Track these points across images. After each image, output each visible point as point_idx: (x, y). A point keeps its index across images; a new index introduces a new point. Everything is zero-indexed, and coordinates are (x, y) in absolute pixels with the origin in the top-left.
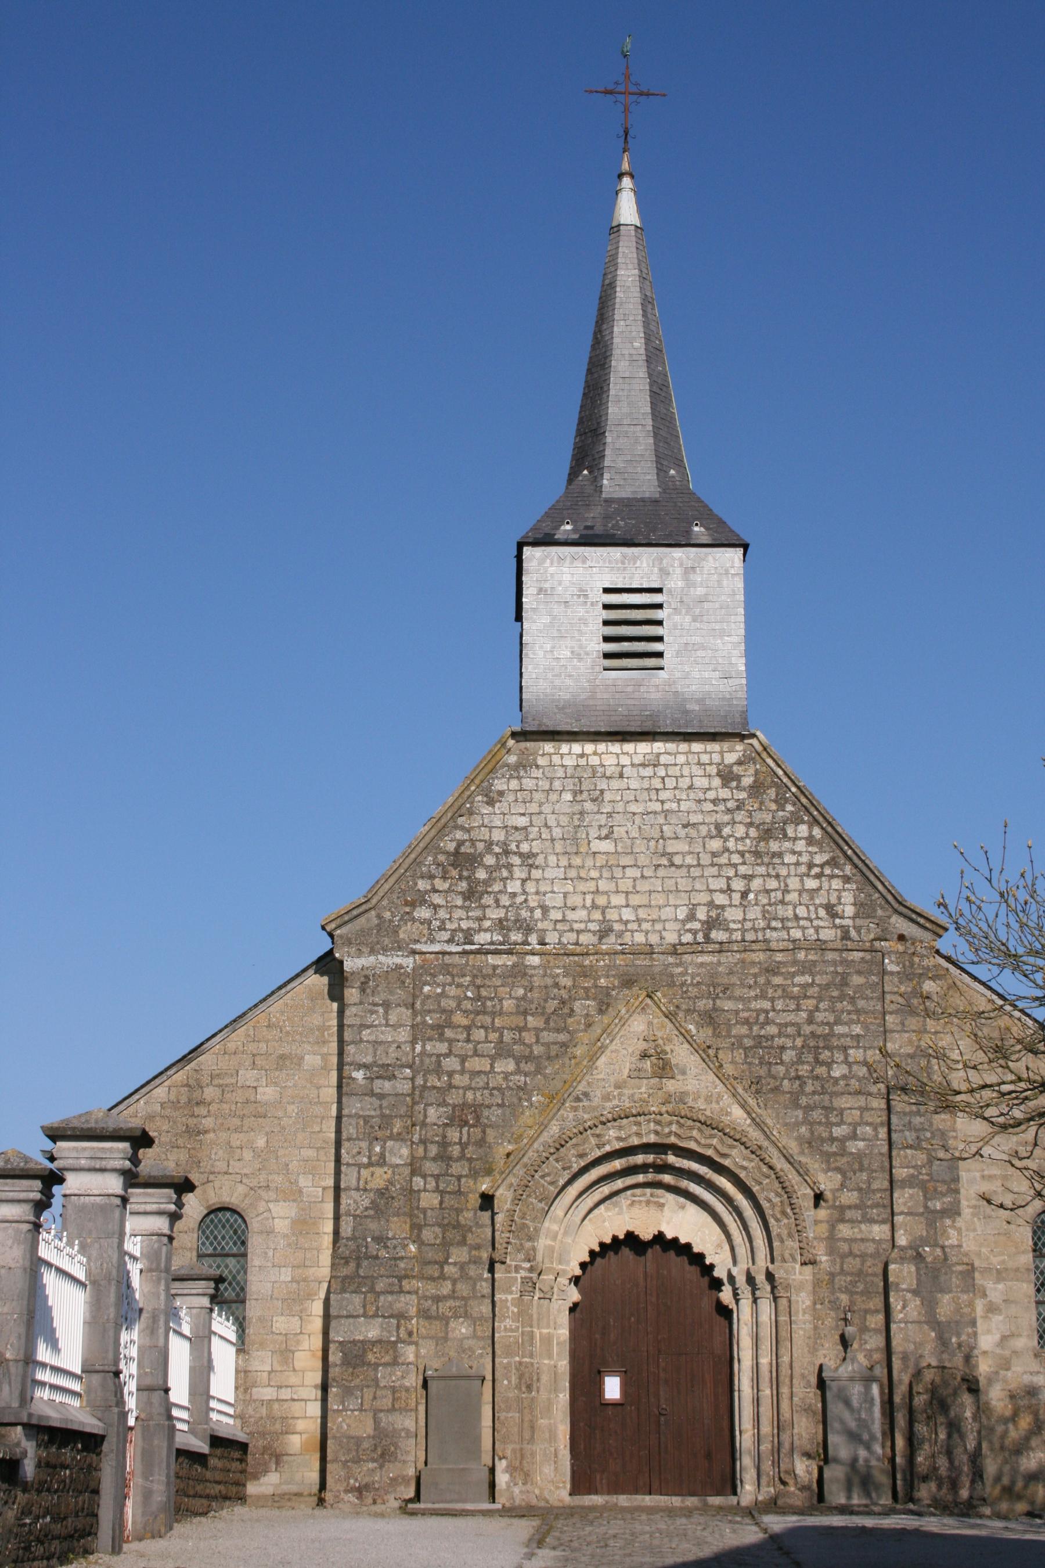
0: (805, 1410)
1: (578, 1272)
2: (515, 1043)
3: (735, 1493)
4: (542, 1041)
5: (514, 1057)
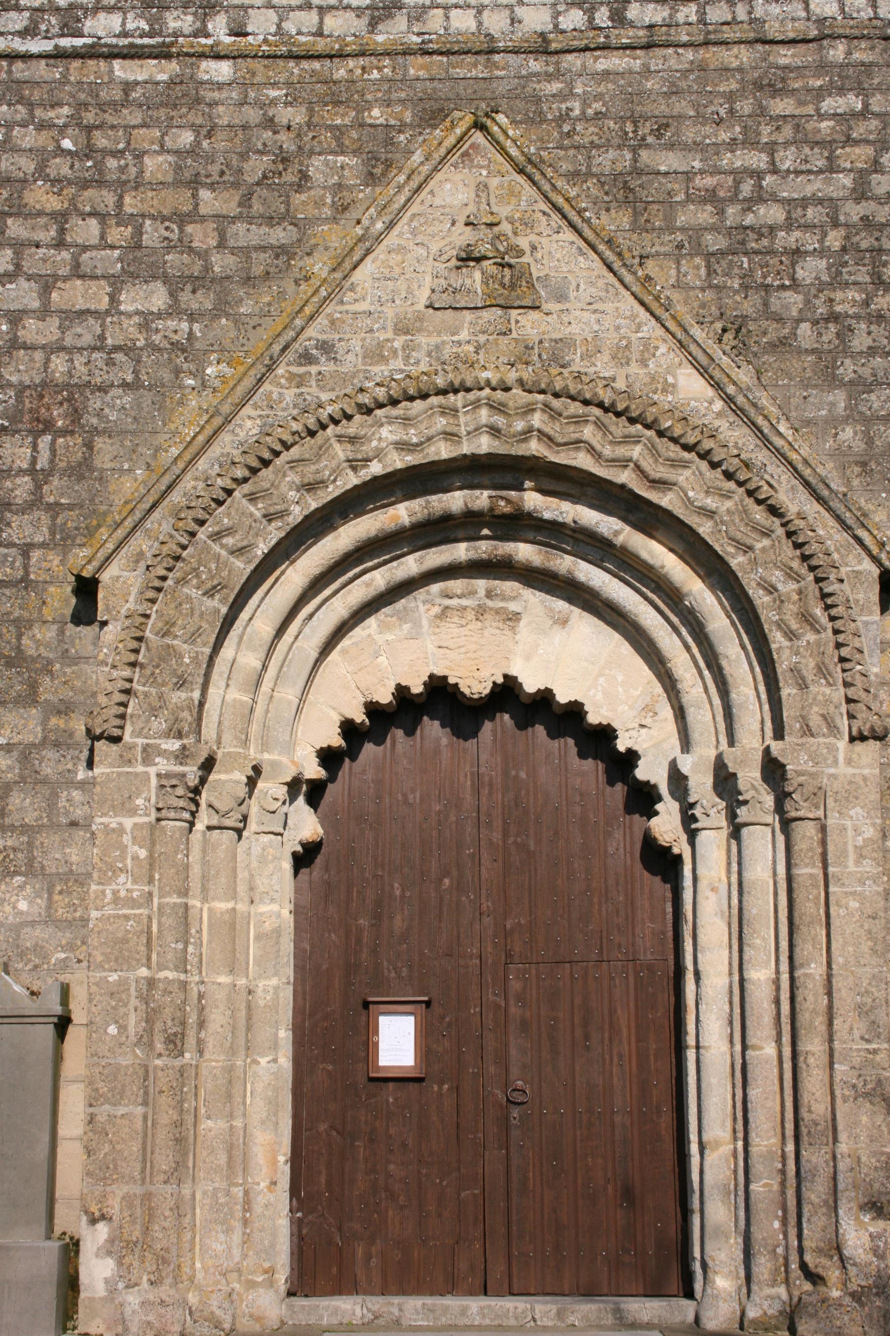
0: (866, 1095)
1: (314, 771)
2: (169, 249)
3: (689, 1294)
4: (231, 243)
5: (166, 279)
